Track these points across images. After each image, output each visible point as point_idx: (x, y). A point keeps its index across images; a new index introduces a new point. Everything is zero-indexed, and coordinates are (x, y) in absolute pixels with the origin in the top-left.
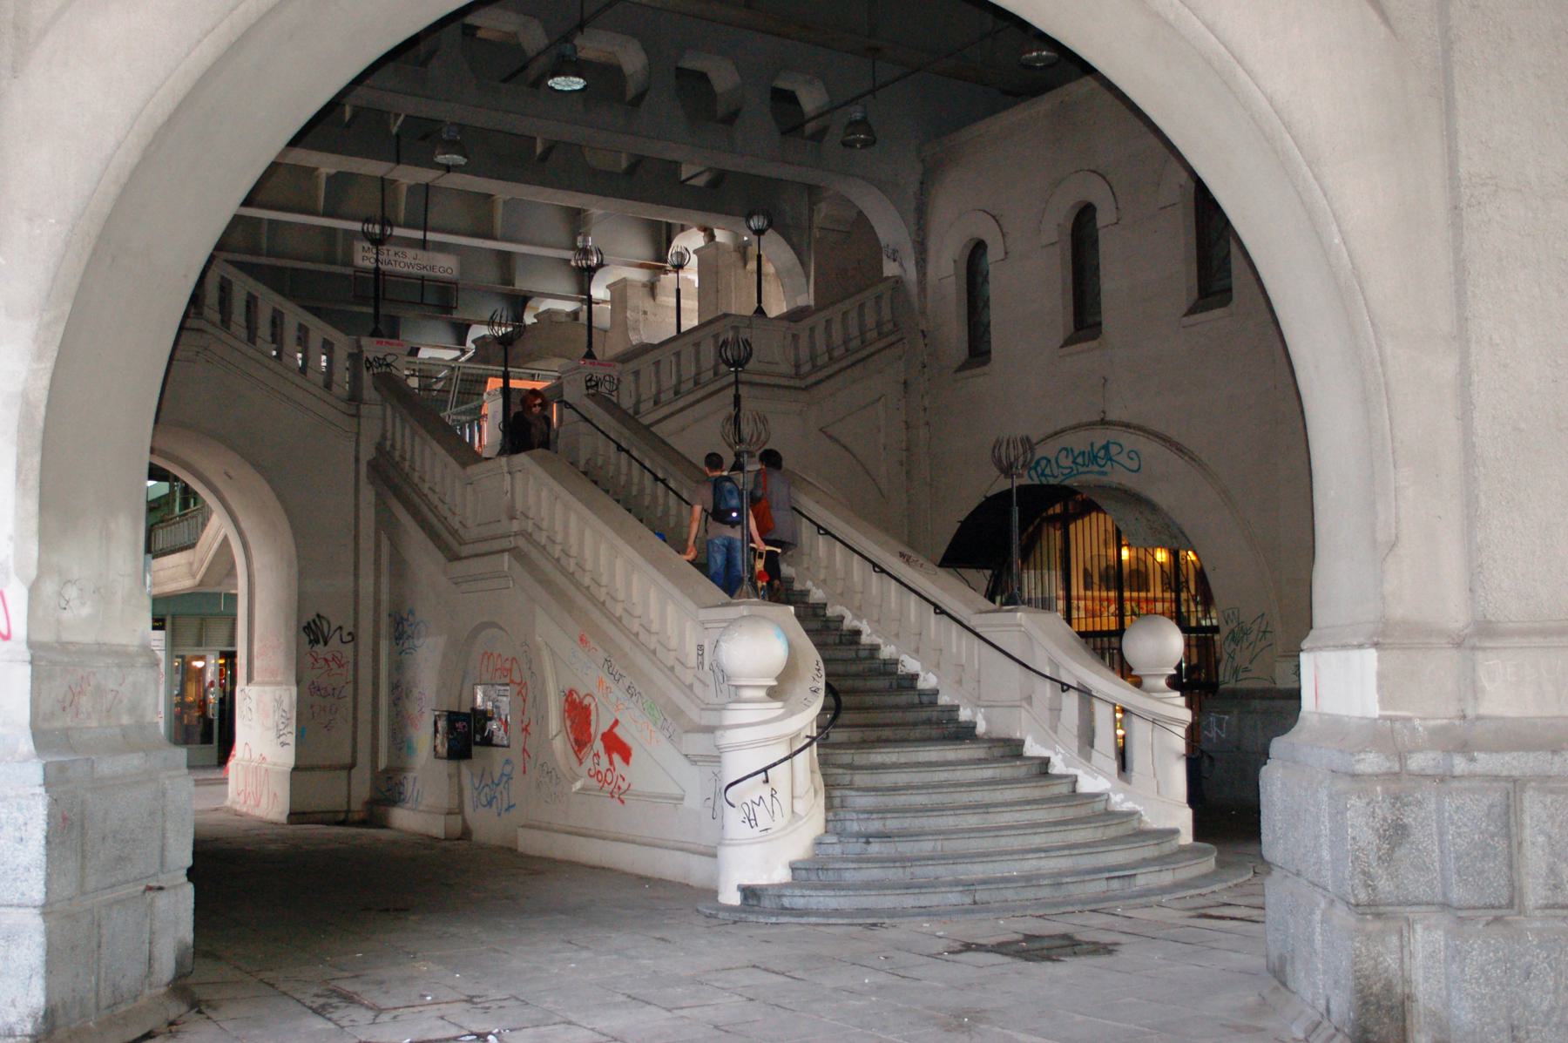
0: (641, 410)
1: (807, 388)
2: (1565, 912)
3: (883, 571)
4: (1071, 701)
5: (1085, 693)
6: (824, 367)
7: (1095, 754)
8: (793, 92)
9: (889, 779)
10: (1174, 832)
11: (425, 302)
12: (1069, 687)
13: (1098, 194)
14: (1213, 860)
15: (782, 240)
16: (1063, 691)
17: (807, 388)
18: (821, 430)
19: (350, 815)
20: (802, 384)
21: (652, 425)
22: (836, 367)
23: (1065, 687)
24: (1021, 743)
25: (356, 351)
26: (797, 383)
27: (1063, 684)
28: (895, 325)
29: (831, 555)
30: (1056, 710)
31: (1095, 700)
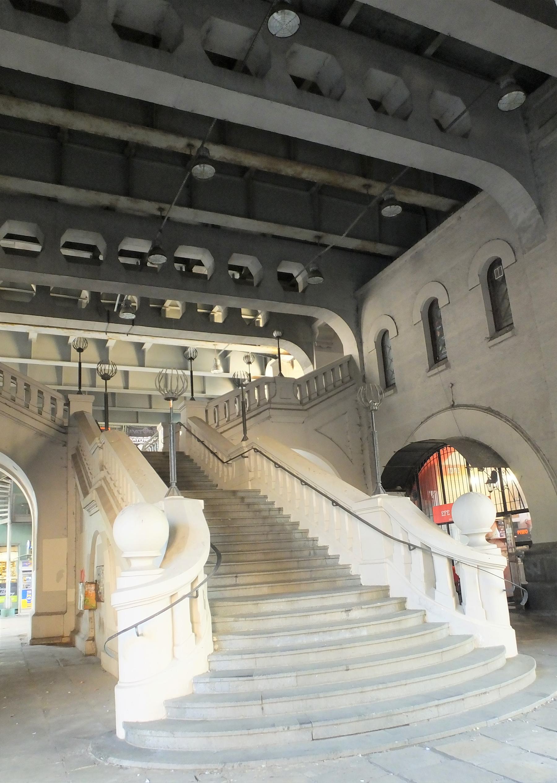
0: (220, 425)
1: (306, 410)
2: (1, 655)
3: (306, 484)
4: (418, 555)
5: (427, 551)
6: (315, 399)
7: (436, 593)
8: (292, 274)
9: (316, 619)
10: (501, 650)
11: (445, 526)
12: (415, 547)
13: (438, 292)
14: (534, 672)
15: (293, 344)
16: (410, 550)
17: (306, 410)
18: (316, 430)
19: (23, 651)
20: (306, 407)
21: (221, 433)
22: (321, 399)
23: (411, 547)
24: (386, 589)
25: (67, 402)
26: (300, 407)
27: (409, 545)
28: (350, 378)
29: (284, 479)
30: (408, 564)
31: (435, 557)
